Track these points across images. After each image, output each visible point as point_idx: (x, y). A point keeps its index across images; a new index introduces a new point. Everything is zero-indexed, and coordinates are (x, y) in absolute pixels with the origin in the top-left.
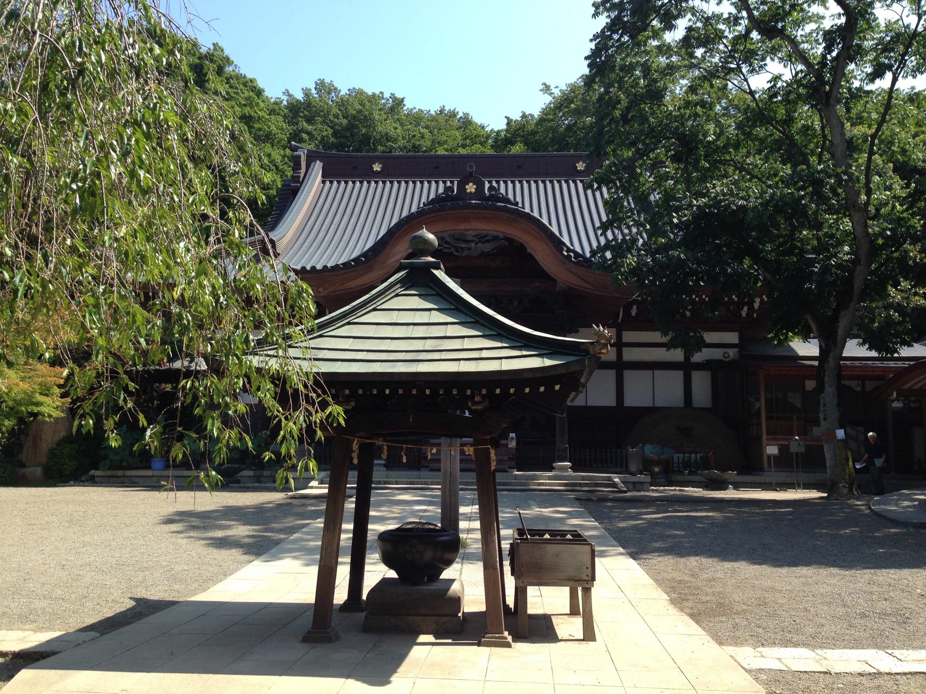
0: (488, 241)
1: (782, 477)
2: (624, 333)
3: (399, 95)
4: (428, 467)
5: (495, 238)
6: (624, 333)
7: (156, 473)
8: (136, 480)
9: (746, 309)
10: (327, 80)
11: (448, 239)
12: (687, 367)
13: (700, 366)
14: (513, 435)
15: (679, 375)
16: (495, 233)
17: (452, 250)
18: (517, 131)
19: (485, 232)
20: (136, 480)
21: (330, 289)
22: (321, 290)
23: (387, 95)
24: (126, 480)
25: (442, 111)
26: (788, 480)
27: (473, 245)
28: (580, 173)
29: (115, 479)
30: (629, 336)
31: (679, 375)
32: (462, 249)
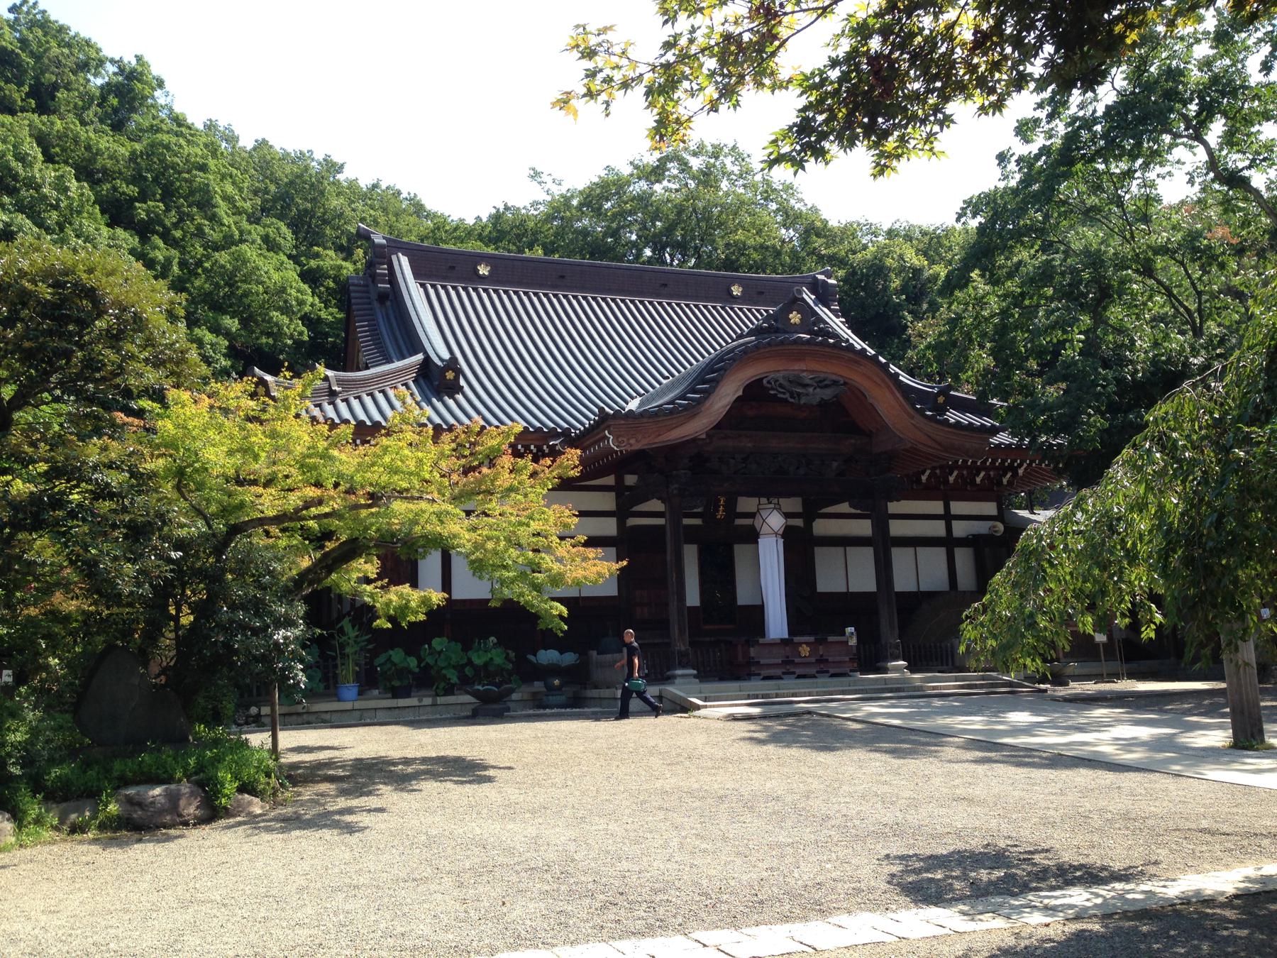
0: (826, 386)
1: (1116, 666)
2: (952, 503)
3: (337, 159)
4: (793, 673)
5: (835, 383)
6: (952, 503)
7: (348, 706)
8: (327, 717)
9: (1009, 475)
10: (222, 124)
11: (782, 381)
12: (949, 543)
13: (963, 542)
14: (850, 630)
15: (941, 553)
16: (834, 377)
17: (787, 396)
18: (503, 228)
19: (822, 376)
20: (327, 717)
21: (645, 441)
22: (632, 441)
23: (319, 156)
24: (312, 718)
25: (375, 186)
26: (1094, 671)
27: (811, 390)
28: (482, 279)
29: (294, 717)
30: (958, 507)
31: (941, 553)
32: (799, 394)
